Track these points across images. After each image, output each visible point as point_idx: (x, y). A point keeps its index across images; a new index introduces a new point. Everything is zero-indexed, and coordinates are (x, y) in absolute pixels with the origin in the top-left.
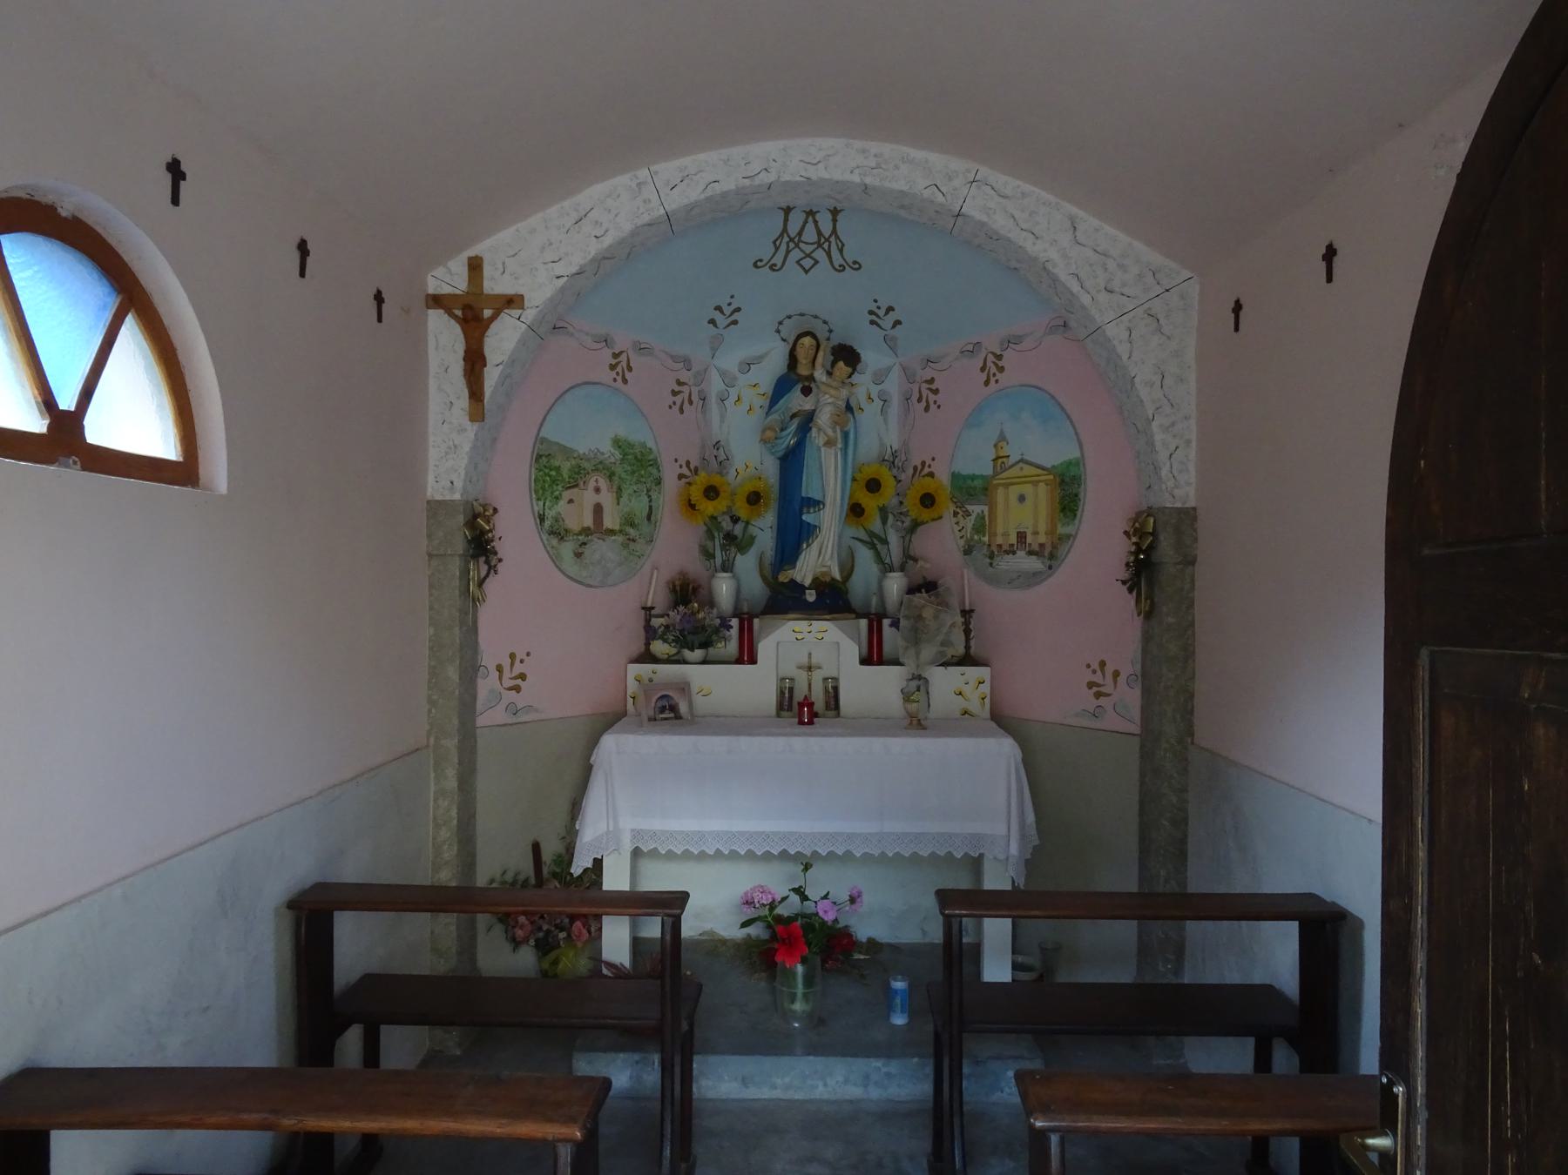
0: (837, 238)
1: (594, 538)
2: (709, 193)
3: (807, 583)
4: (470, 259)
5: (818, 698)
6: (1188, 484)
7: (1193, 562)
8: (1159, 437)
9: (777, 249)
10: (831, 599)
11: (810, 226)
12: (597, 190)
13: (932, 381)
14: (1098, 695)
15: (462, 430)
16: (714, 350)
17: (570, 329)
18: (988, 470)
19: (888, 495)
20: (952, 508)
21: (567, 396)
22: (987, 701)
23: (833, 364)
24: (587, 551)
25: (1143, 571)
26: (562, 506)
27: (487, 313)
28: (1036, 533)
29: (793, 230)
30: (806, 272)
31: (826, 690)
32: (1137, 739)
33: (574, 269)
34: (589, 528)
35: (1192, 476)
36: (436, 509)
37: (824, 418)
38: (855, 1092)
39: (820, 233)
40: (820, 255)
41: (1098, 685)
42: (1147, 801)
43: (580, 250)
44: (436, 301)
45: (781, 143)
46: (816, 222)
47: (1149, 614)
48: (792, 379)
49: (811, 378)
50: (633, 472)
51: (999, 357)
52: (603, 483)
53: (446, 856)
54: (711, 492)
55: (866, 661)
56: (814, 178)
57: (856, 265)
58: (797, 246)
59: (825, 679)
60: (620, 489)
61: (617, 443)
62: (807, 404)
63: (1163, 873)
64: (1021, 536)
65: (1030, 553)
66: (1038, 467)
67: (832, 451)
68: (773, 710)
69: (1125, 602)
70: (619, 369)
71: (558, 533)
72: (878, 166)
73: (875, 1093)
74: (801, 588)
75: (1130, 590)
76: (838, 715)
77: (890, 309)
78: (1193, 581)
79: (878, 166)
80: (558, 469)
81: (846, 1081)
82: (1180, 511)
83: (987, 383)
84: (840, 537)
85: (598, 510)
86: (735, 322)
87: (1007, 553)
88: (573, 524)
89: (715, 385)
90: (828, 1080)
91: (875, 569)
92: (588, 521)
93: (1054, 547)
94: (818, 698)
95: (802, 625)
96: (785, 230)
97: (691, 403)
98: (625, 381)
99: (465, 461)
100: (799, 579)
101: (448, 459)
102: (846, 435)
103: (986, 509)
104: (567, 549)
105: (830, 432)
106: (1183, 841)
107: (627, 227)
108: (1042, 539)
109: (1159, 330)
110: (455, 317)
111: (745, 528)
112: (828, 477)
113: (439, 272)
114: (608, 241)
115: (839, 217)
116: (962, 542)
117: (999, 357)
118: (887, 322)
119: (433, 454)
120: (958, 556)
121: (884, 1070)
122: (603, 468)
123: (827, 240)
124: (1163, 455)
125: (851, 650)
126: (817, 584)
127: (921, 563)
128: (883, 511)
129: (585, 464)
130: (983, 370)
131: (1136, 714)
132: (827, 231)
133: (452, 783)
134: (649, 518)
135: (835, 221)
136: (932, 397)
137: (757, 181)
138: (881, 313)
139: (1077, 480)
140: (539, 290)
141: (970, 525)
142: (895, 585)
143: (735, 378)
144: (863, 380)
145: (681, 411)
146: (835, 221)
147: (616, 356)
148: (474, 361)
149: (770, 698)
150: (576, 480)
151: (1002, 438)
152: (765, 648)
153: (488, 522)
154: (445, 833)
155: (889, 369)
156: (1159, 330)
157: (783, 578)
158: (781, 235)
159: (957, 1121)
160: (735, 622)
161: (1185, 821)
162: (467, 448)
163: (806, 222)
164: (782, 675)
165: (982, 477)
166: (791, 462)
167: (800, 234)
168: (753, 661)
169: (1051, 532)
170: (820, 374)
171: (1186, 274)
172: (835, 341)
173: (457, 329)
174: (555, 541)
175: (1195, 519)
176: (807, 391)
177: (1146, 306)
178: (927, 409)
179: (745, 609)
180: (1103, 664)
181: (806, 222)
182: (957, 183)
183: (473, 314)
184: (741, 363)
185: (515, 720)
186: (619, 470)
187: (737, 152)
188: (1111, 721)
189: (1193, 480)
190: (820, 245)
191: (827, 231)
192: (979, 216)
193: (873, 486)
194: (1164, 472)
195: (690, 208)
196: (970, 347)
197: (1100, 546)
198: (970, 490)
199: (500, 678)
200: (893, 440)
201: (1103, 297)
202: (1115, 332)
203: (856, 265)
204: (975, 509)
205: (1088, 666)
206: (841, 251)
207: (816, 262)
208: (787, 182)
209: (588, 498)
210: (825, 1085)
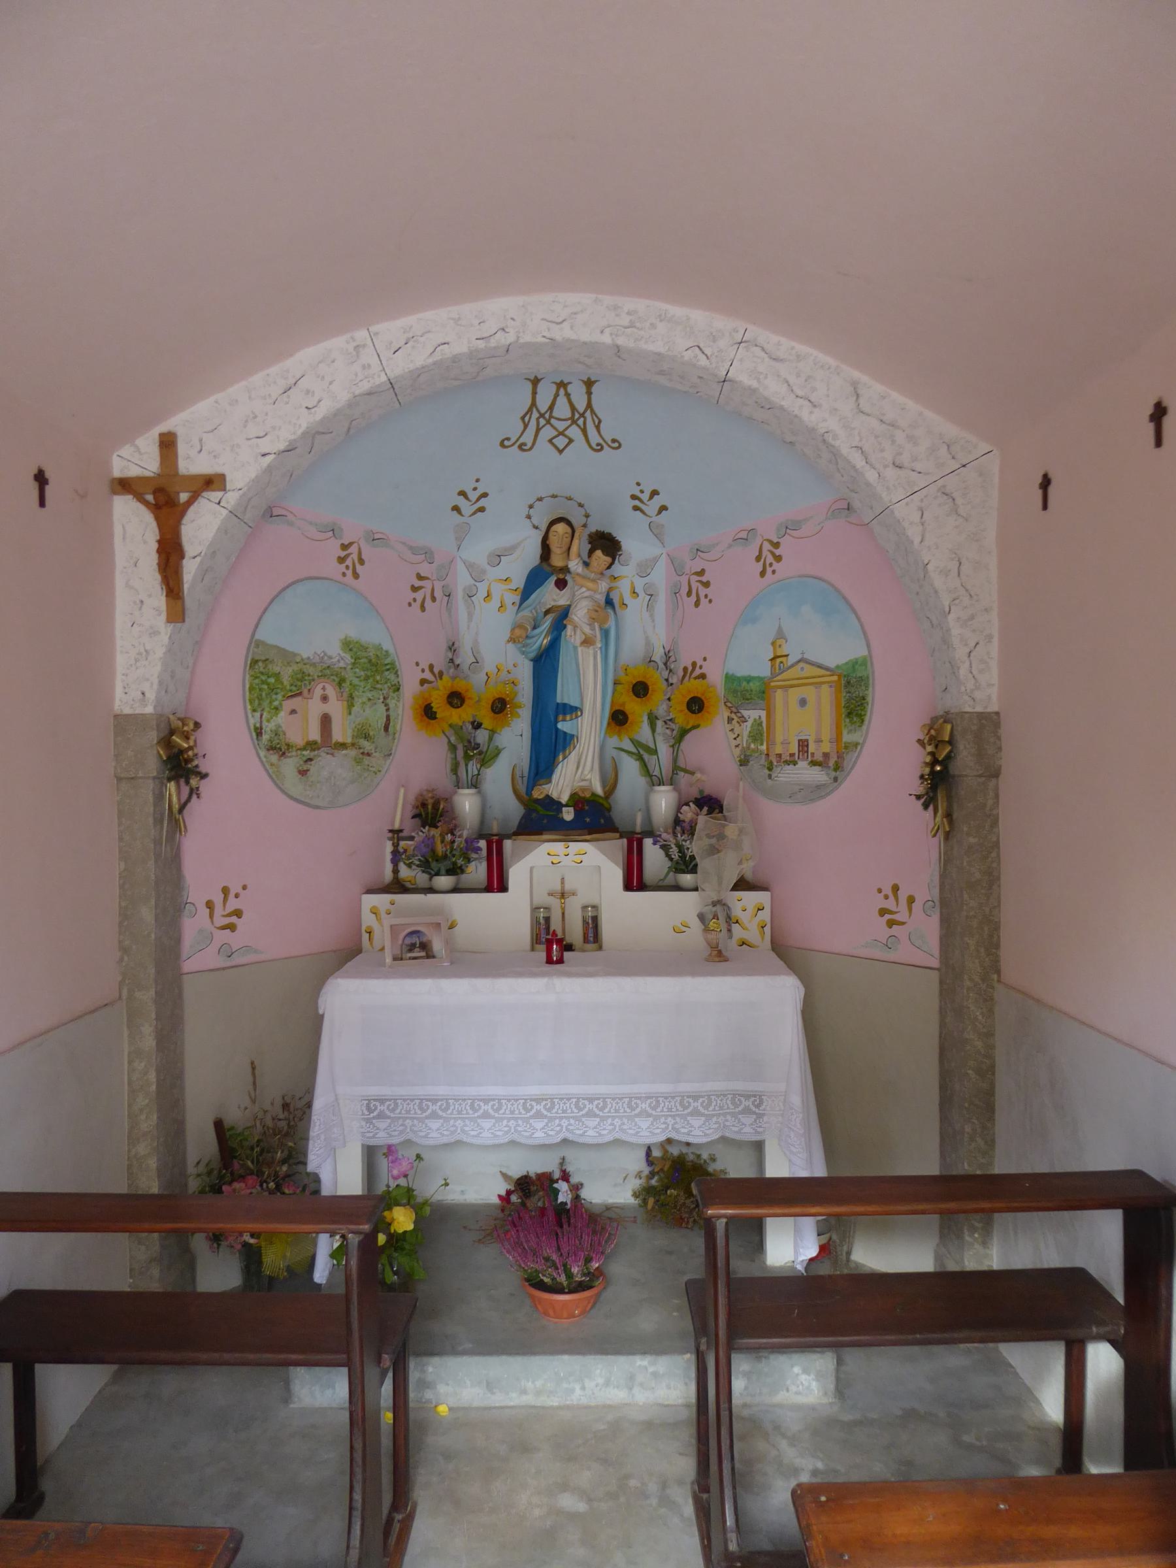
0: (593, 412)
1: (322, 752)
2: (437, 357)
3: (564, 799)
4: (161, 435)
5: (575, 933)
6: (990, 685)
7: (996, 775)
8: (956, 631)
9: (526, 426)
10: (592, 817)
11: (562, 400)
12: (307, 355)
13: (702, 573)
14: (891, 923)
15: (154, 633)
16: (460, 541)
17: (290, 517)
18: (764, 671)
19: (658, 702)
20: (726, 714)
21: (288, 590)
22: (768, 929)
23: (591, 552)
24: (313, 768)
25: (938, 782)
26: (282, 718)
27: (184, 497)
28: (819, 741)
29: (543, 404)
30: (561, 452)
31: (585, 922)
32: (936, 974)
33: (282, 446)
34: (315, 743)
35: (994, 675)
36: (124, 724)
37: (580, 615)
38: (617, 1395)
39: (573, 408)
40: (574, 432)
41: (891, 912)
42: (947, 1046)
43: (288, 424)
44: (124, 485)
45: (520, 300)
46: (568, 395)
47: (949, 831)
48: (546, 570)
49: (565, 570)
50: (367, 678)
51: (776, 545)
52: (331, 691)
53: (144, 1127)
54: (456, 699)
55: (628, 886)
56: (558, 338)
57: (616, 444)
58: (548, 422)
59: (585, 907)
60: (351, 697)
61: (347, 645)
62: (561, 599)
63: (968, 1129)
64: (803, 745)
65: (814, 763)
66: (820, 666)
67: (591, 651)
68: (528, 947)
69: (921, 821)
70: (349, 562)
71: (279, 748)
72: (632, 325)
73: (641, 1397)
74: (558, 806)
75: (926, 806)
76: (600, 948)
77: (654, 493)
78: (997, 796)
79: (632, 325)
80: (277, 675)
81: (607, 1383)
82: (981, 716)
83: (763, 574)
84: (602, 748)
85: (326, 720)
86: (482, 509)
87: (787, 763)
88: (295, 737)
89: (462, 579)
90: (587, 1383)
91: (642, 781)
92: (315, 734)
93: (840, 756)
94: (575, 933)
95: (558, 847)
96: (534, 404)
97: (434, 599)
98: (356, 575)
99: (158, 668)
100: (555, 796)
101: (139, 661)
102: (606, 634)
103: (763, 714)
104: (290, 766)
105: (587, 629)
106: (990, 1092)
107: (344, 397)
108: (826, 747)
109: (955, 511)
110: (146, 503)
111: (491, 739)
112: (587, 682)
113: (126, 451)
114: (320, 413)
115: (594, 389)
116: (737, 752)
117: (776, 545)
118: (652, 507)
119: (121, 661)
120: (733, 768)
121: (651, 1370)
122: (328, 672)
123: (582, 415)
124: (961, 652)
125: (615, 874)
126: (577, 801)
127: (698, 775)
128: (653, 719)
129: (311, 670)
130: (758, 559)
131: (936, 951)
132: (581, 406)
133: (149, 1042)
134: (386, 728)
135: (589, 393)
136: (703, 591)
137: (493, 343)
138: (645, 497)
139: (863, 681)
140: (242, 474)
141: (746, 734)
142: (663, 802)
143: (484, 572)
144: (626, 571)
145: (423, 608)
146: (589, 393)
147: (345, 547)
148: (170, 553)
149: (523, 930)
150: (299, 688)
151: (781, 635)
152: (516, 874)
153: (187, 738)
154: (142, 1101)
155: (656, 560)
156: (955, 511)
157: (537, 794)
158: (530, 410)
159: (726, 1465)
160: (482, 844)
161: (992, 1068)
162: (160, 652)
163: (557, 395)
164: (536, 904)
165: (759, 679)
166: (545, 664)
167: (551, 408)
168: (503, 888)
169: (838, 738)
170: (575, 565)
171: (984, 447)
172: (593, 528)
173: (148, 517)
174: (274, 758)
175: (997, 725)
176: (561, 584)
177: (940, 483)
178: (697, 604)
179: (495, 830)
180: (896, 888)
181: (557, 395)
182: (722, 343)
183: (167, 498)
184: (489, 556)
185: (229, 964)
186: (349, 676)
187: (468, 310)
188: (904, 953)
189: (995, 681)
190: (574, 422)
191: (581, 406)
192: (746, 380)
193: (641, 689)
194: (963, 671)
195: (416, 375)
196: (744, 535)
197: (890, 756)
198: (746, 693)
199: (211, 916)
200: (660, 639)
201: (890, 473)
202: (907, 513)
203: (616, 444)
204: (752, 714)
205: (880, 891)
206: (598, 428)
207: (571, 441)
208: (528, 344)
209: (314, 708)
210: (583, 1388)
